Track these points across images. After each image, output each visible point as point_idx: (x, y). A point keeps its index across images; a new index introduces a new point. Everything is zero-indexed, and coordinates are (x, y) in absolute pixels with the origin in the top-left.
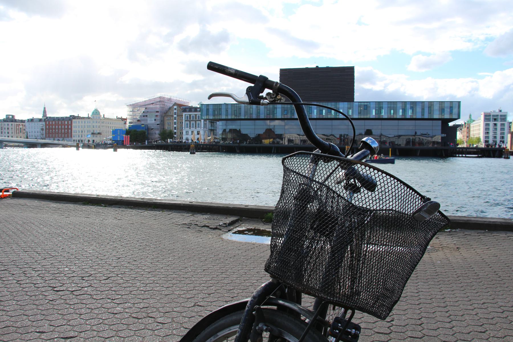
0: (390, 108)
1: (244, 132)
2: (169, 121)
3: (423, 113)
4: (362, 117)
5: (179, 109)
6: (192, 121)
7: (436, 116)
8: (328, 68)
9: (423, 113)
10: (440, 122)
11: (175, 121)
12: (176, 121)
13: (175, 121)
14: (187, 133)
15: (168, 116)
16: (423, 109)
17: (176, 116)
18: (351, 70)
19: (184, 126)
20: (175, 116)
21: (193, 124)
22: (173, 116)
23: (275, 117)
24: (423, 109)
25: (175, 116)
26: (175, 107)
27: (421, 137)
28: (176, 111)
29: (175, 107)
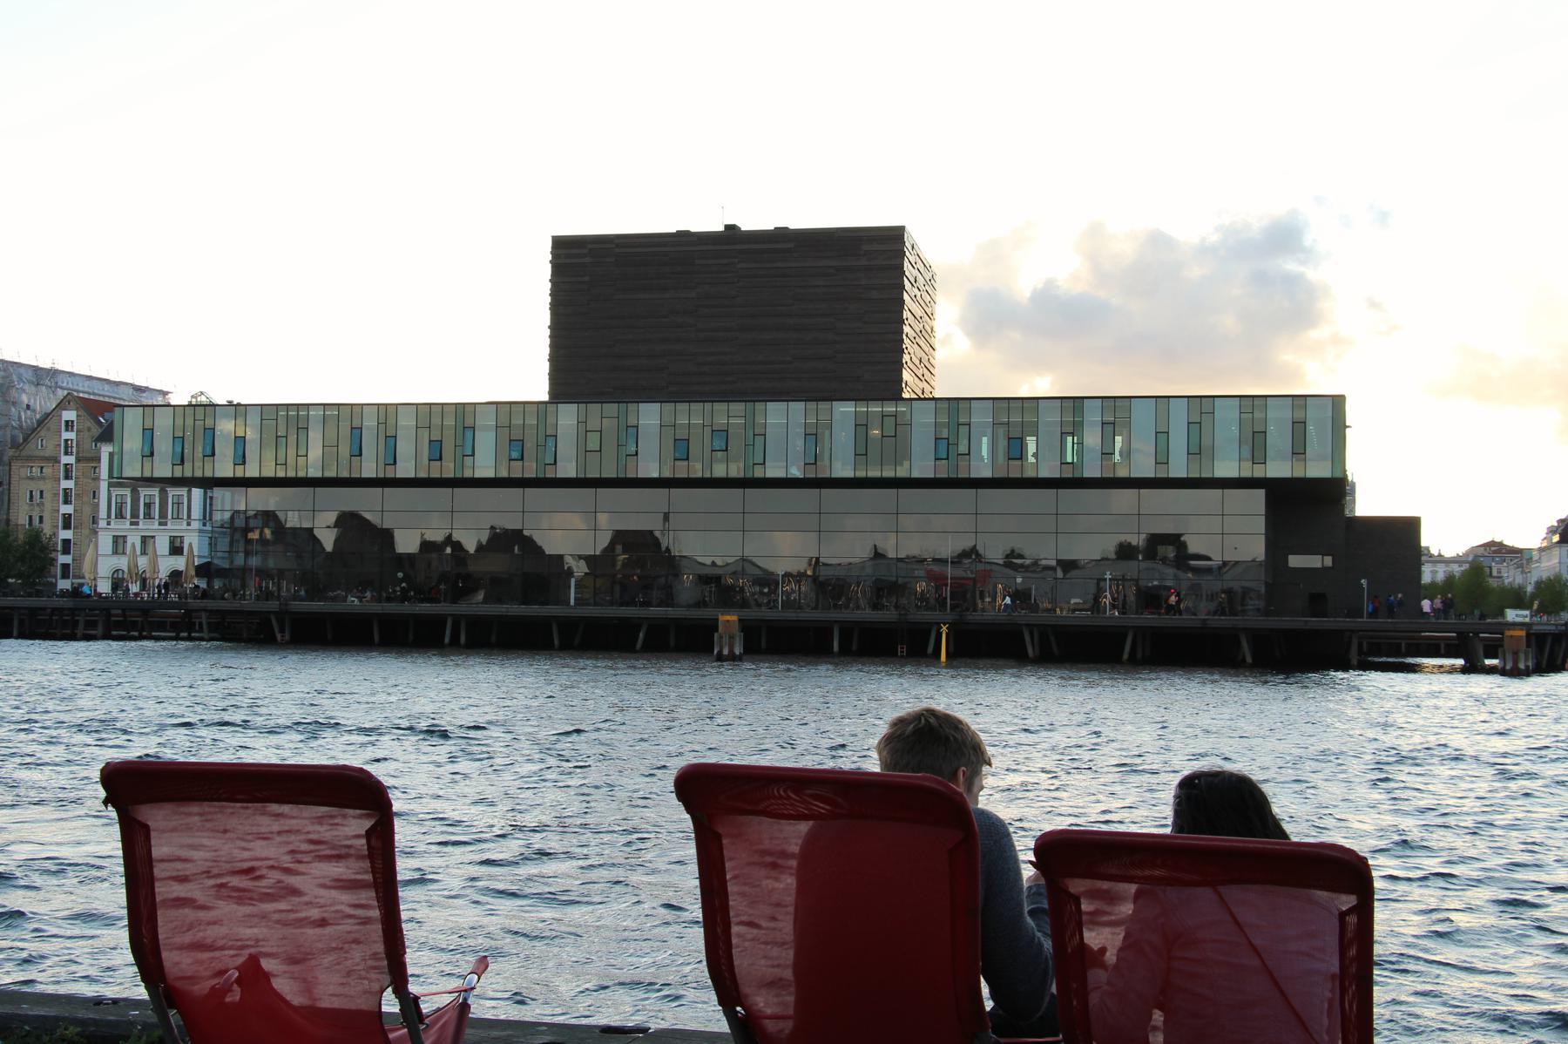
0: (1109, 428)
1: (1300, 817)
2: (36, 487)
3: (1162, 459)
4: (874, 473)
5: (89, 423)
6: (149, 490)
7: (1226, 468)
8: (781, 235)
9: (1162, 459)
10: (1260, 494)
11: (65, 484)
12: (70, 484)
13: (65, 484)
14: (119, 543)
15: (30, 458)
16: (1162, 435)
17: (71, 459)
18: (563, 246)
19: (103, 513)
20: (65, 459)
21: (148, 506)
22: (57, 460)
23: (468, 474)
24: (1162, 435)
25: (65, 459)
26: (69, 415)
27: (368, 504)
28: (72, 435)
29: (69, 415)
